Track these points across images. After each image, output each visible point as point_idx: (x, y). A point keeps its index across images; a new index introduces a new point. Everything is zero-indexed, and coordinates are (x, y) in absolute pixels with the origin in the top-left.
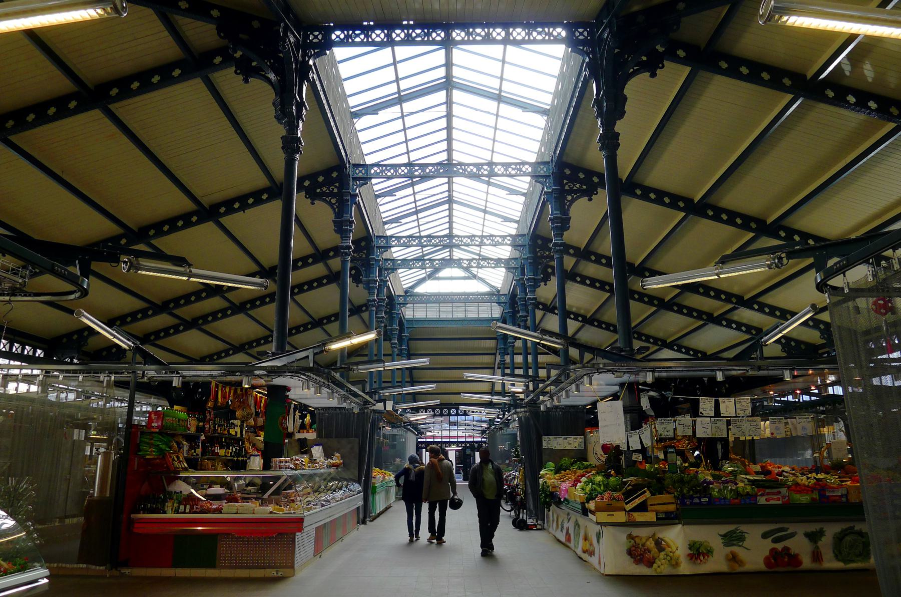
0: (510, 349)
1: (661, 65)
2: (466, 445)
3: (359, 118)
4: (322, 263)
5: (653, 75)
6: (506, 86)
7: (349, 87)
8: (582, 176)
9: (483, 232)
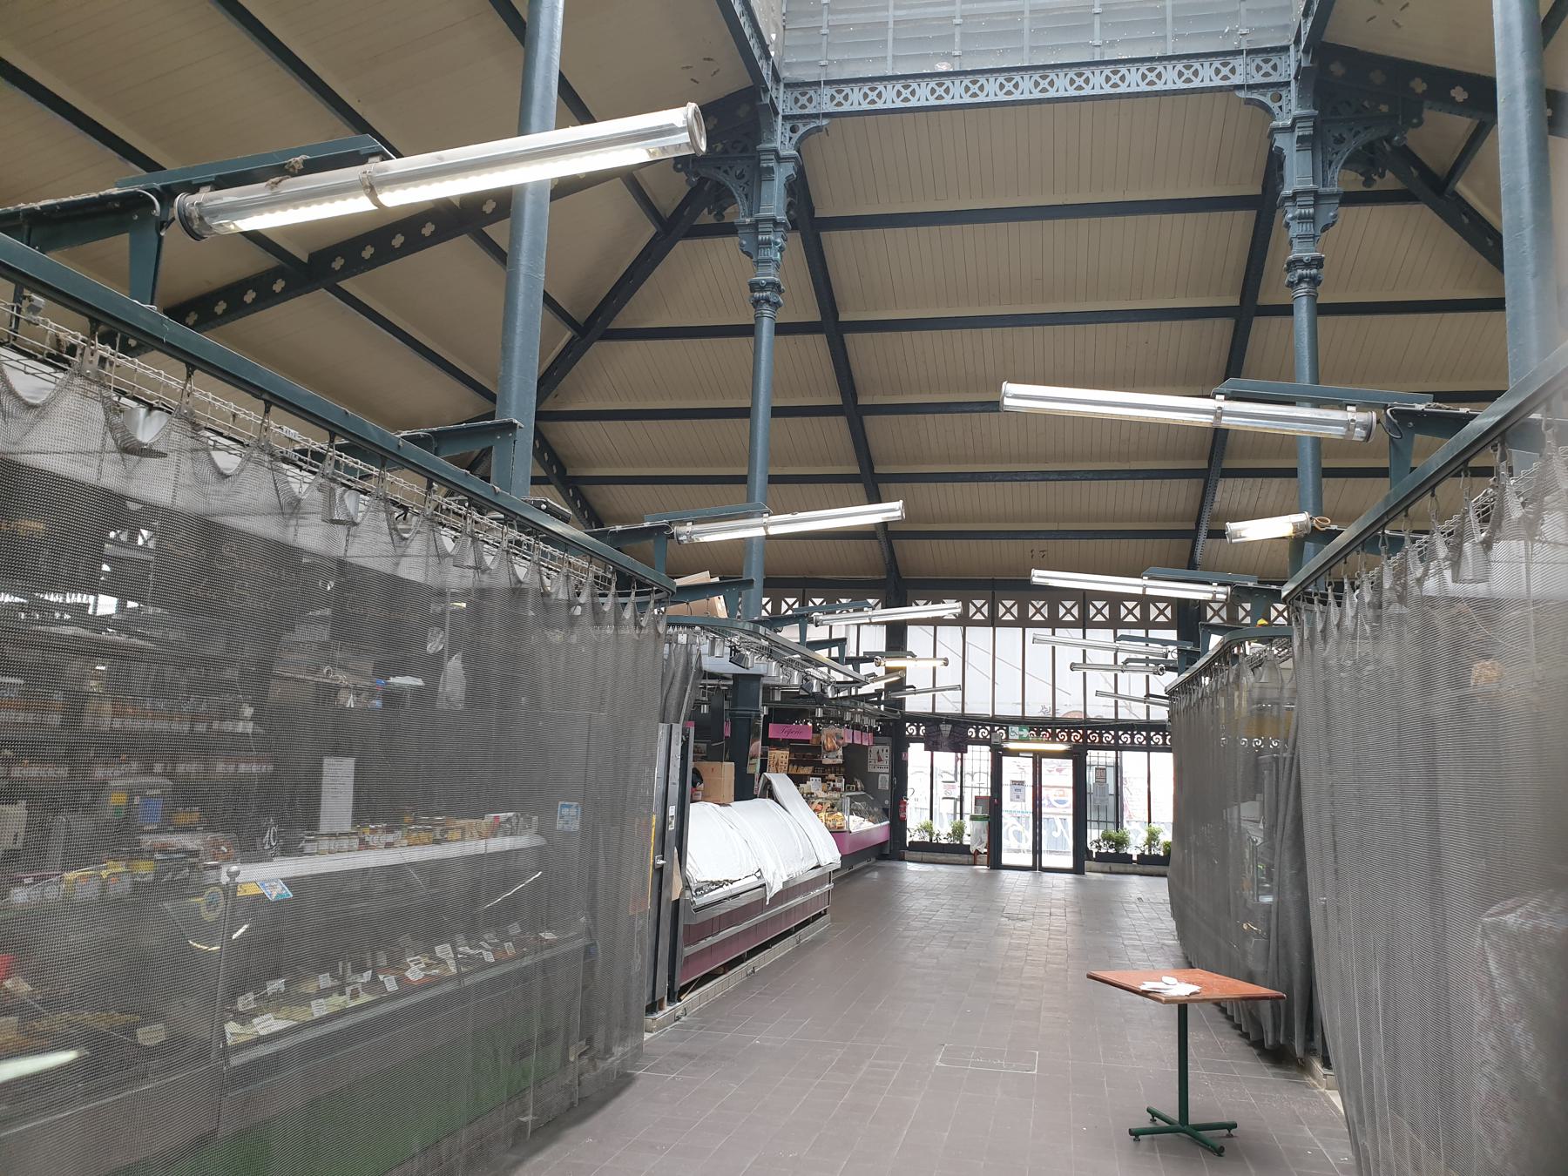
2: (1085, 736)
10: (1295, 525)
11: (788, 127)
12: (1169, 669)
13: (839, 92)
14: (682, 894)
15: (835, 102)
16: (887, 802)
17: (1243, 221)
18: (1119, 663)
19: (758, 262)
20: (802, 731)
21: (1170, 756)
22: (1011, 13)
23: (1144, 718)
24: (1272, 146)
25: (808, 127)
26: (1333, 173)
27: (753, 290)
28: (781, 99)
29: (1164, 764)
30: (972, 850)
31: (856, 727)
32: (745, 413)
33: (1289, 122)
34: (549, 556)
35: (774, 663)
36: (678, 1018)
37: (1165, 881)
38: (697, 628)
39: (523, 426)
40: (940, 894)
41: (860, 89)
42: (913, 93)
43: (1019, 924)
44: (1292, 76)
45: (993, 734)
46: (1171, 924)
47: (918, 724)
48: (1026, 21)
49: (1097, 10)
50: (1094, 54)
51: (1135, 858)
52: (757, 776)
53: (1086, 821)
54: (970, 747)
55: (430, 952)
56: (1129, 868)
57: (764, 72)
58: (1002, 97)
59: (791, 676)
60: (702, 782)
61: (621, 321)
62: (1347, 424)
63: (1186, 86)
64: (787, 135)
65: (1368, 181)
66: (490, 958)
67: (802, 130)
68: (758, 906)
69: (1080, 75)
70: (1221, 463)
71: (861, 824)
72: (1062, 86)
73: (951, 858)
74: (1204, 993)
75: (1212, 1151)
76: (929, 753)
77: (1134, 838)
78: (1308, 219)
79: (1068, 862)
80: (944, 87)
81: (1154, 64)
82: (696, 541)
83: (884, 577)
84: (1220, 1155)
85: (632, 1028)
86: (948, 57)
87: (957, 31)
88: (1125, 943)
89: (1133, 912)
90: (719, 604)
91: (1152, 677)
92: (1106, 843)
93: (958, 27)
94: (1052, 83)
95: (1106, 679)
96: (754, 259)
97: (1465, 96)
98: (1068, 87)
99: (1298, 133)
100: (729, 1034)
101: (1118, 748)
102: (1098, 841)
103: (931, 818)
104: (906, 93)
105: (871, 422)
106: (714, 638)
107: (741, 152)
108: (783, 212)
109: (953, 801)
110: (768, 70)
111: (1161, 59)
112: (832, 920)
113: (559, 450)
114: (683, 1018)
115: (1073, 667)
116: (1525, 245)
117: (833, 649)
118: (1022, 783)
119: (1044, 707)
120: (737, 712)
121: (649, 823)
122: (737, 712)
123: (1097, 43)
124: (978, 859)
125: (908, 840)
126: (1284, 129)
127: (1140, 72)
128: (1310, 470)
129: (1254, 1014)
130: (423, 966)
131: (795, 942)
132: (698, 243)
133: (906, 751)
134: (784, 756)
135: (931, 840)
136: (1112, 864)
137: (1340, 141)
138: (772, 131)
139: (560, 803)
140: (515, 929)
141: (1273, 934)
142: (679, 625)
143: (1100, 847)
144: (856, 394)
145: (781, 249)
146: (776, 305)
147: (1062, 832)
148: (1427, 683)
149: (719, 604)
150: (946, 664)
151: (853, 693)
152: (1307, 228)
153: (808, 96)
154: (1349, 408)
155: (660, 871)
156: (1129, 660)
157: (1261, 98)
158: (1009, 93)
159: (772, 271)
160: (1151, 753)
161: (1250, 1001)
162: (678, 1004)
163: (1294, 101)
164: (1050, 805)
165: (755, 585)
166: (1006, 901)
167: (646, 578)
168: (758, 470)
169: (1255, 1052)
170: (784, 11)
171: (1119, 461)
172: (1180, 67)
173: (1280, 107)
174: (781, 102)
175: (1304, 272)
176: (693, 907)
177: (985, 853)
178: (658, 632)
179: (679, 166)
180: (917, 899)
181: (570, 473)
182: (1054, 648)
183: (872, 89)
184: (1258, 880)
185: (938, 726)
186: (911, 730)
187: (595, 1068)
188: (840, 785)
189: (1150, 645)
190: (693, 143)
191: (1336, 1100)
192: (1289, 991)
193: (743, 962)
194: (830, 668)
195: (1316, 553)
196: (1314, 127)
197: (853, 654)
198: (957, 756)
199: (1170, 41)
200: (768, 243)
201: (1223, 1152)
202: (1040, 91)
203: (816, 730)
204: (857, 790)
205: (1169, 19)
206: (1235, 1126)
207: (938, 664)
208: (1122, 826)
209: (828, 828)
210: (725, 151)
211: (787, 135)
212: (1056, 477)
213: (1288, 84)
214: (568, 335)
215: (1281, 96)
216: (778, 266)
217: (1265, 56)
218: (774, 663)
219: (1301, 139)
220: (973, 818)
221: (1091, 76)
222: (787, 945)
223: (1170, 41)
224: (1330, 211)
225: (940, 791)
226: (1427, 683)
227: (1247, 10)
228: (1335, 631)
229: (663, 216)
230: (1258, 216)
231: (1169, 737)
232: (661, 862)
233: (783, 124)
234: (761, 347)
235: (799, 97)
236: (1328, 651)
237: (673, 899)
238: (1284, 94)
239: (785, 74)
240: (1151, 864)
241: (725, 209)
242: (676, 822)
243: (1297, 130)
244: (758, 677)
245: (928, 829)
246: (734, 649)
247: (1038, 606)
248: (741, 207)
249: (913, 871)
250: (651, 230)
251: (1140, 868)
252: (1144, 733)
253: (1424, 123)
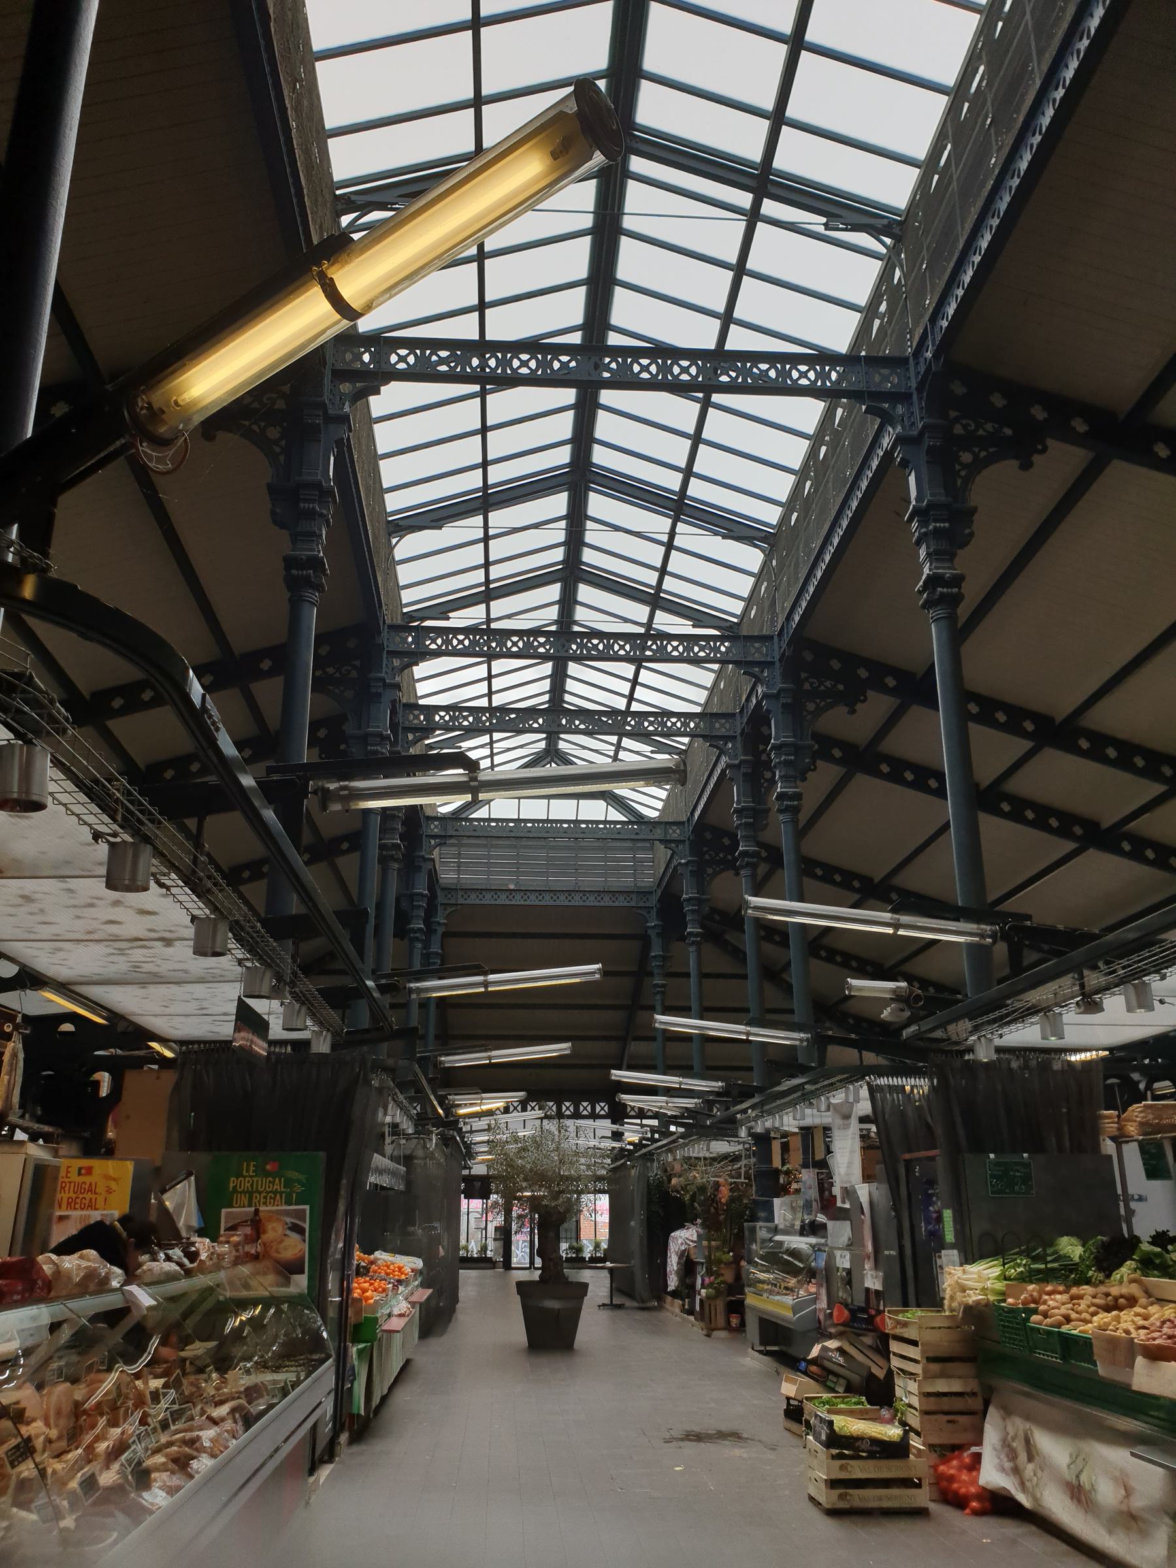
0: (658, 997)
1: (862, 698)
3: (402, 537)
5: (1026, 465)
6: (669, 584)
7: (390, 472)
8: (835, 665)
9: (727, 319)
219: (784, 706)
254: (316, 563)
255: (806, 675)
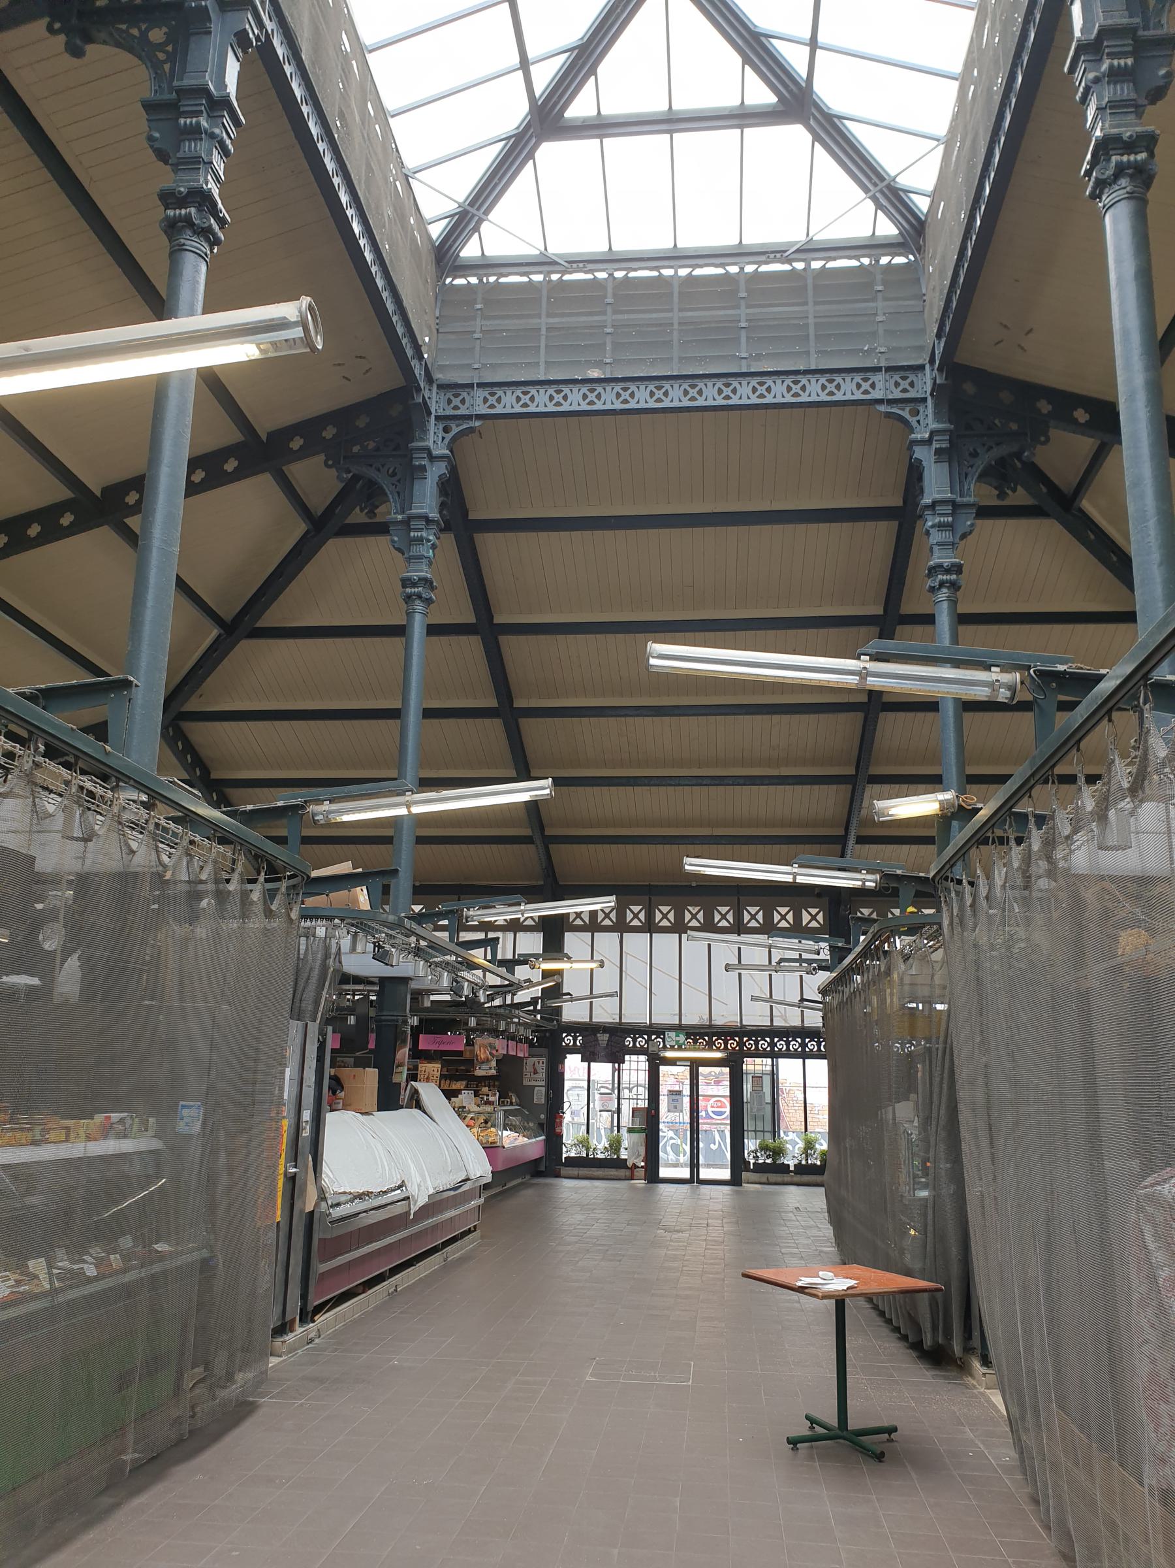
2: (741, 1044)
4: (566, 934)
10: (941, 802)
11: (441, 427)
12: (821, 968)
13: (492, 394)
14: (317, 1205)
15: (487, 405)
16: (542, 1116)
17: (883, 533)
18: (773, 963)
19: (410, 558)
20: (454, 1042)
21: (824, 1062)
22: (661, 325)
23: (798, 1023)
24: (911, 458)
25: (461, 428)
26: (969, 485)
27: (404, 586)
28: (434, 400)
29: (819, 1070)
30: (629, 1164)
31: (512, 1037)
32: (394, 714)
33: (927, 435)
34: (171, 832)
35: (422, 963)
36: (311, 1341)
37: (821, 1191)
38: (337, 921)
39: (139, 684)
40: (595, 1209)
41: (513, 393)
42: (565, 398)
43: (675, 1236)
44: (928, 393)
45: (650, 1042)
46: (828, 1231)
47: (575, 1034)
48: (675, 333)
49: (743, 324)
50: (741, 366)
51: (792, 1168)
52: (403, 1085)
53: (744, 1131)
54: (627, 1057)
55: (22, 1268)
56: (787, 1178)
57: (417, 372)
58: (652, 404)
59: (441, 976)
60: (342, 1089)
61: (269, 619)
62: (991, 685)
63: (829, 398)
64: (440, 435)
65: (1002, 495)
66: (91, 1271)
67: (455, 430)
68: (402, 1220)
69: (727, 385)
70: (867, 769)
71: (515, 1139)
72: (710, 395)
73: (607, 1173)
74: (861, 1287)
75: (873, 1458)
76: (586, 1064)
77: (791, 1148)
78: (943, 527)
79: (726, 1174)
80: (596, 393)
81: (799, 377)
82: (333, 821)
83: (542, 883)
84: (880, 1461)
85: (254, 1352)
86: (600, 364)
87: (609, 340)
88: (783, 1250)
89: (790, 1221)
90: (362, 897)
91: (805, 976)
92: (763, 1153)
93: (610, 336)
94: (700, 393)
95: (761, 989)
96: (406, 555)
97: (1087, 417)
98: (716, 397)
99: (935, 445)
100: (366, 1356)
101: (774, 1055)
102: (755, 1152)
103: (588, 1132)
104: (558, 398)
105: (526, 723)
106: (356, 933)
107: (395, 450)
108: (436, 510)
109: (610, 1113)
110: (421, 370)
111: (806, 372)
112: (482, 1237)
113: (204, 753)
114: (317, 1341)
115: (728, 968)
116: (1149, 535)
117: (510, 1002)
118: (679, 1093)
119: (701, 1018)
120: (383, 1018)
121: (279, 1129)
122: (383, 1018)
123: (742, 357)
124: (636, 1173)
125: (564, 1156)
126: (922, 442)
127: (785, 384)
128: (954, 769)
129: (913, 1315)
130: (12, 1283)
131: (442, 1260)
132: (349, 542)
133: (563, 1063)
134: (436, 1070)
135: (587, 1155)
136: (769, 1174)
137: (975, 455)
138: (425, 431)
139: (181, 1103)
140: (126, 1242)
141: (930, 1228)
142: (317, 918)
143: (758, 1157)
144: (511, 696)
145: (434, 547)
146: (429, 601)
147: (719, 1143)
148: (1079, 959)
149: (362, 897)
150: (602, 966)
151: (508, 1002)
152: (946, 536)
153: (461, 398)
154: (993, 669)
155: (292, 1179)
156: (782, 960)
157: (900, 412)
158: (659, 400)
159: (425, 568)
160: (807, 1061)
161: (908, 1295)
162: (311, 1325)
163: (931, 416)
164: (708, 1116)
165: (401, 874)
166: (663, 1213)
167: (277, 858)
168: (409, 766)
169: (914, 1355)
170: (438, 315)
171: (769, 767)
172: (823, 380)
173: (918, 422)
174: (434, 403)
175: (945, 577)
176: (328, 1219)
177: (642, 1167)
178: (291, 919)
179: (330, 462)
180: (572, 1215)
181: (213, 776)
182: (709, 945)
183: (525, 393)
184: (914, 1174)
185: (595, 1036)
186: (568, 1040)
187: (214, 1398)
188: (495, 1098)
189: (803, 942)
190: (307, 340)
191: (997, 1399)
192: (948, 1285)
193: (385, 1281)
194: (485, 970)
195: (961, 829)
196: (950, 441)
197: (510, 957)
198: (614, 1067)
199: (813, 356)
200: (420, 540)
201: (884, 1457)
202: (689, 400)
203: (470, 1043)
204: (512, 1104)
205: (812, 337)
206: (895, 1429)
207: (593, 965)
208: (779, 1135)
209: (481, 1144)
210: (377, 449)
211: (440, 435)
212: (709, 782)
213: (924, 400)
214: (215, 632)
215: (918, 412)
216: (430, 563)
217: (903, 374)
218: (422, 963)
219: (938, 452)
220: (630, 1130)
221: (738, 386)
222: (435, 1260)
223: (813, 356)
224: (967, 521)
225: (597, 1104)
226: (1079, 959)
227: (885, 330)
228: (984, 904)
229: (313, 513)
230: (900, 526)
231: (823, 1044)
232: (294, 1170)
233: (435, 424)
234: (412, 642)
235: (452, 398)
236: (981, 935)
237: (307, 1211)
238: (921, 409)
239: (438, 376)
240: (807, 1174)
241: (378, 507)
242: (312, 1128)
243: (934, 442)
244: (405, 980)
245: (585, 1143)
246: (377, 945)
247: (694, 912)
248: (393, 504)
249: (569, 1188)
250: (301, 528)
251: (797, 1178)
252: (799, 1040)
253: (1051, 441)
254: (203, 199)
255: (889, 914)
